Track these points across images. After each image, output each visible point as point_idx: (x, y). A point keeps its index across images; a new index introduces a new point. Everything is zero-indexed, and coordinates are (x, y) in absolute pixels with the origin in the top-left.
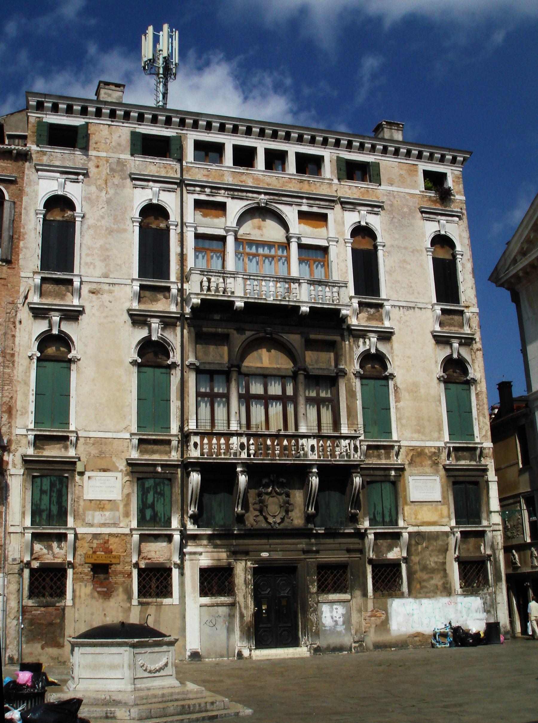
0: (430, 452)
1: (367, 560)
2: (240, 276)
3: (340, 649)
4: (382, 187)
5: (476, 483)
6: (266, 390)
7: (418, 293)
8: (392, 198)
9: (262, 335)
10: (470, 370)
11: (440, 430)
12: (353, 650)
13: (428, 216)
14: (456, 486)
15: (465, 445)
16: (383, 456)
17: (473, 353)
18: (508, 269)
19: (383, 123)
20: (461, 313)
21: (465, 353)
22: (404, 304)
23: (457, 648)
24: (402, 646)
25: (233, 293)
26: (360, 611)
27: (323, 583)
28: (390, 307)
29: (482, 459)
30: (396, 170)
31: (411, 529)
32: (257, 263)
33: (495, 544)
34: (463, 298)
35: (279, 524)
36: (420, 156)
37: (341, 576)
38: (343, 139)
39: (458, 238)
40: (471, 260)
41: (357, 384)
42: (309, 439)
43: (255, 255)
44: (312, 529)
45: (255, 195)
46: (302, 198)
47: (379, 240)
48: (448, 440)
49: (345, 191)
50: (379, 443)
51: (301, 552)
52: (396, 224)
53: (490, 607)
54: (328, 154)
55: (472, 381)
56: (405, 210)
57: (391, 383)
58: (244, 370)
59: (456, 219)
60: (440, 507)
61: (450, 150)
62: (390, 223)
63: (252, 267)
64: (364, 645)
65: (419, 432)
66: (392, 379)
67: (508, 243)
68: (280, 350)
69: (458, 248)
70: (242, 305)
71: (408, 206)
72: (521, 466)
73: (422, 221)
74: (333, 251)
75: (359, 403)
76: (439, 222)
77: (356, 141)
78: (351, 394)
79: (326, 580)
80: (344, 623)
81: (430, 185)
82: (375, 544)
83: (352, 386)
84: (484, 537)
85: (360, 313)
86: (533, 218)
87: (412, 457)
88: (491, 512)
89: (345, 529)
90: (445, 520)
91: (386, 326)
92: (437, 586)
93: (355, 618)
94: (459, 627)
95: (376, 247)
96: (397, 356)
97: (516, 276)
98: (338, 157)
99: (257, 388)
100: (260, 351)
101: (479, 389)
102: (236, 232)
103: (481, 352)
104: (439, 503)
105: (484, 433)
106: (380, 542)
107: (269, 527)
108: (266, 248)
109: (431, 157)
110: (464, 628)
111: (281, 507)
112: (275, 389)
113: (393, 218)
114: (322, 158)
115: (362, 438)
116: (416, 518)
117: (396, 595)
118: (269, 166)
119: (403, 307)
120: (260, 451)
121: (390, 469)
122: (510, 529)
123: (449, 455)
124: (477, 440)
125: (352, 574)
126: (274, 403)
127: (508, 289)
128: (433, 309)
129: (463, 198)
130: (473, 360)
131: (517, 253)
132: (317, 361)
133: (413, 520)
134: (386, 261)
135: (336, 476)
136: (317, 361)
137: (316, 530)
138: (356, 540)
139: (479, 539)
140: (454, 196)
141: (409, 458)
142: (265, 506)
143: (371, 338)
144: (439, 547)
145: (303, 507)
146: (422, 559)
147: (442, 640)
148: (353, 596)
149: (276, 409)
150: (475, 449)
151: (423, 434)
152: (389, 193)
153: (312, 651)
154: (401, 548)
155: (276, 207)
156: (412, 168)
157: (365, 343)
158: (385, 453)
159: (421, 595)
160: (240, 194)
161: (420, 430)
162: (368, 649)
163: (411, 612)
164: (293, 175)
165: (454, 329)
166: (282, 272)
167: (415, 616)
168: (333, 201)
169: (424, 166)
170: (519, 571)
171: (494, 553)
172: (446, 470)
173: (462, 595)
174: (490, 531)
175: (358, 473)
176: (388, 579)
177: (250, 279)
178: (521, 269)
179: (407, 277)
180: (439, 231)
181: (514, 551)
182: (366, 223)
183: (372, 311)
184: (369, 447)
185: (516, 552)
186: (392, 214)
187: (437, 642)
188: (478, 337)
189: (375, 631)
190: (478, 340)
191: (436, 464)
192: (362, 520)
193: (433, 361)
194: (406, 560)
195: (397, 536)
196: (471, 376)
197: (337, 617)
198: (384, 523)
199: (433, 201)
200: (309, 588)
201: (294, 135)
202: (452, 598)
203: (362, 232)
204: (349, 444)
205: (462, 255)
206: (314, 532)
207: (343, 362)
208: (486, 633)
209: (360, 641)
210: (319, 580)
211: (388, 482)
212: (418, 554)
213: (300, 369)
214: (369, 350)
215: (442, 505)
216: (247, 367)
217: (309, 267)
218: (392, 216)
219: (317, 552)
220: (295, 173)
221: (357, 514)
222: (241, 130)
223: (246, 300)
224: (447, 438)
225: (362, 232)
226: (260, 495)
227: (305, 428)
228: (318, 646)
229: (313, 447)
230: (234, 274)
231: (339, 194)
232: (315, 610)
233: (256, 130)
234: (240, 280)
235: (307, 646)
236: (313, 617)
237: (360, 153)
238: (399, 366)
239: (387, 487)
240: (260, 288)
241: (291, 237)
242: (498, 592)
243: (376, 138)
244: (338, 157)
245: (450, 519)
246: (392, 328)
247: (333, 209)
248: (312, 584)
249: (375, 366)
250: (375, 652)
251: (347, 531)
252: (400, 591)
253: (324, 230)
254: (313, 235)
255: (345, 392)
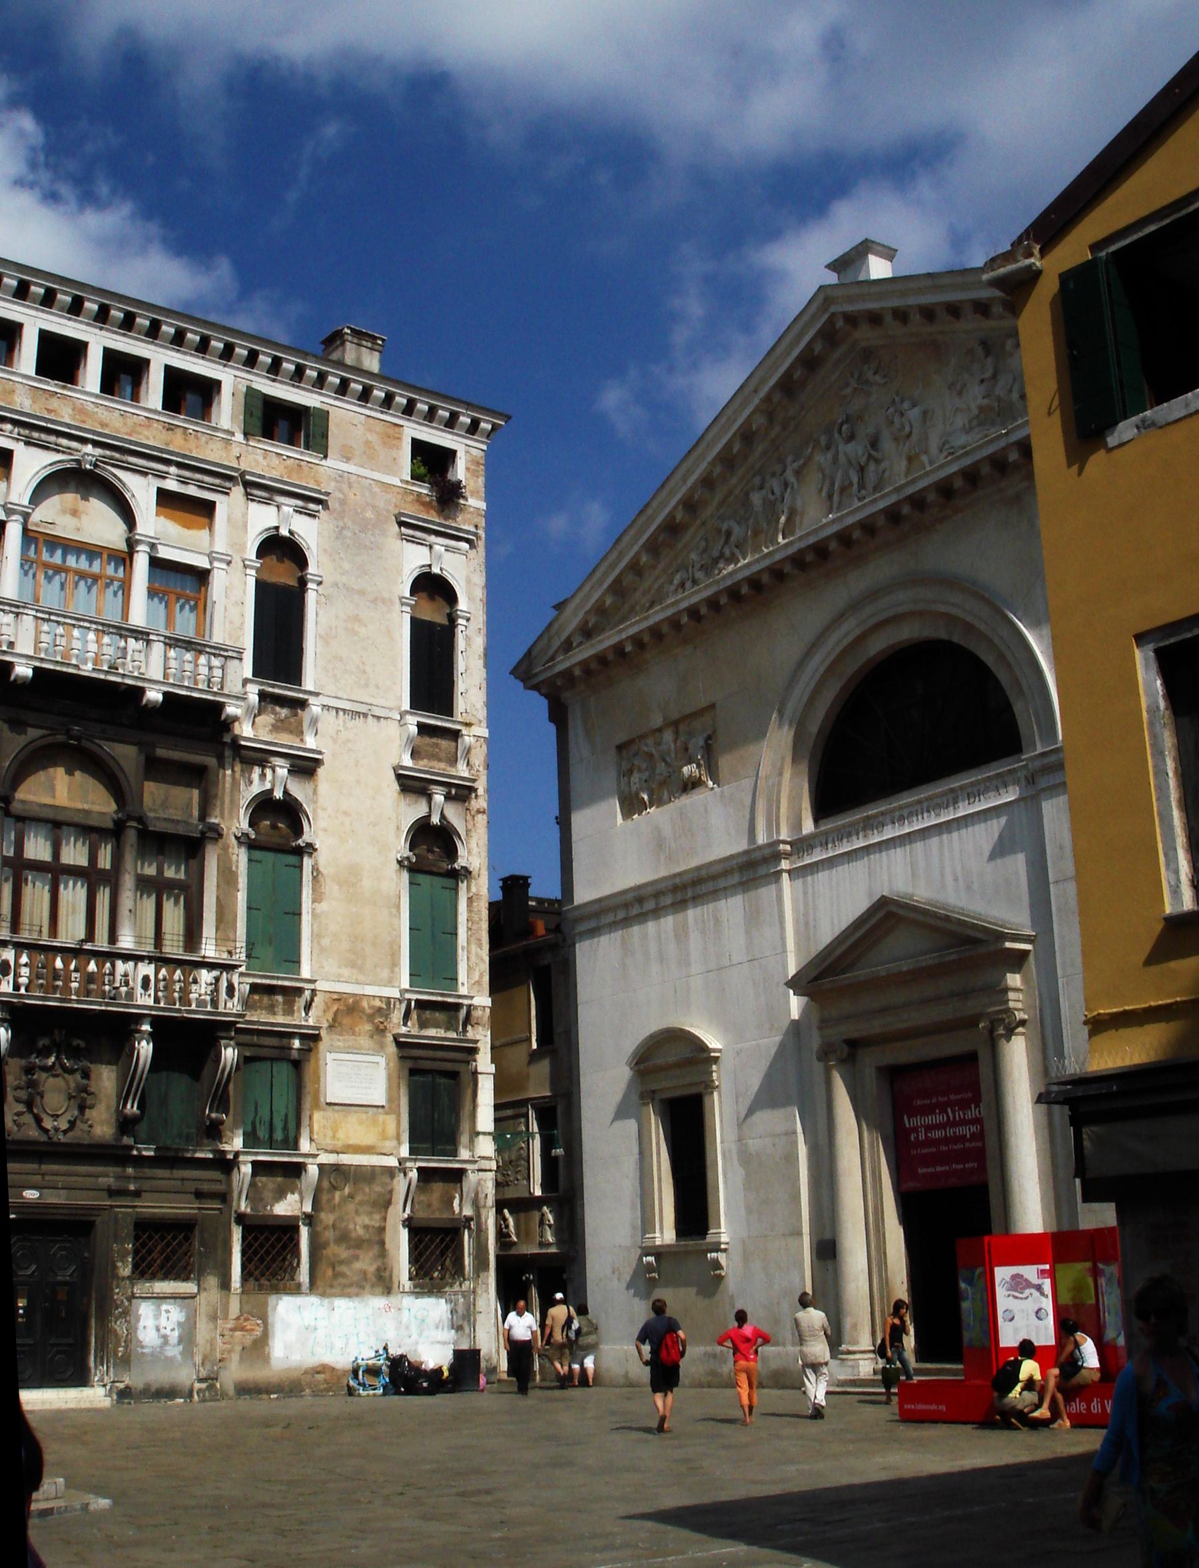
0: (371, 1007)
1: (234, 1215)
2: (30, 612)
3: (170, 1393)
4: (329, 462)
5: (454, 1075)
6: (56, 854)
7: (377, 687)
8: (345, 487)
9: (61, 738)
10: (461, 851)
11: (395, 964)
12: (196, 1396)
13: (410, 532)
14: (416, 1078)
15: (440, 999)
16: (279, 1009)
17: (469, 817)
18: (552, 659)
19: (347, 331)
20: (455, 735)
21: (454, 815)
22: (347, 706)
23: (396, 1397)
24: (291, 1391)
25: (11, 644)
26: (213, 1318)
27: (143, 1259)
28: (319, 709)
29: (469, 1028)
30: (360, 432)
31: (325, 1158)
32: (62, 586)
33: (482, 1196)
34: (460, 705)
35: (65, 1132)
36: (409, 410)
37: (180, 1244)
38: (264, 353)
39: (463, 583)
40: (484, 631)
41: (241, 858)
42: (140, 964)
43: (58, 570)
44: (131, 1148)
45: (74, 444)
46: (168, 462)
47: (312, 569)
48: (407, 986)
49: (256, 461)
50: (274, 982)
51: (105, 1194)
52: (348, 541)
53: (463, 1320)
54: (231, 381)
55: (463, 872)
56: (369, 514)
57: (307, 862)
58: (16, 807)
59: (465, 546)
60: (381, 1118)
61: (469, 405)
62: (337, 538)
63: (51, 595)
64: (218, 1385)
65: (353, 965)
66: (310, 855)
67: (560, 607)
68: (93, 775)
69: (463, 605)
70: (29, 673)
71: (374, 507)
72: (535, 1046)
73: (399, 542)
74: (219, 581)
75: (242, 897)
76: (431, 547)
77: (288, 361)
78: (227, 877)
79: (150, 1252)
80: (180, 1341)
81: (422, 470)
82: (252, 1185)
83: (230, 860)
84: (461, 1181)
85: (259, 713)
86: (616, 565)
87: (336, 1014)
88: (478, 1134)
89: (195, 1151)
90: (389, 1145)
91: (308, 746)
92: (365, 1273)
93: (203, 1331)
94: (403, 1357)
95: (303, 583)
96: (324, 809)
97: (567, 674)
98: (250, 389)
99: (37, 848)
100: (51, 770)
101: (474, 889)
102: (26, 516)
103: (485, 817)
104: (380, 1110)
105: (476, 978)
106: (262, 1180)
107: (44, 1138)
108: (83, 557)
109: (430, 416)
110: (412, 1358)
111: (70, 1097)
112: (75, 854)
113: (343, 528)
114: (217, 384)
115: (242, 969)
116: (334, 1137)
117: (284, 1289)
118: (109, 386)
119: (344, 710)
120: (41, 981)
121: (291, 1035)
122: (510, 1166)
123: (407, 1016)
124: (463, 991)
125: (203, 1244)
126: (71, 883)
127: (546, 696)
128: (401, 723)
129: (483, 505)
130: (468, 831)
131: (575, 629)
132: (167, 803)
133: (328, 1141)
134: (321, 613)
135: (187, 1041)
136: (165, 805)
137: (138, 1149)
138: (216, 1175)
139: (452, 1185)
140: (465, 498)
141: (330, 1016)
142: (38, 1094)
143: (278, 769)
144: (373, 1196)
145: (114, 1102)
146: (341, 1218)
147: (369, 1380)
148: (202, 1286)
149: (74, 895)
150: (457, 1007)
151: (361, 969)
152: (342, 476)
153: (115, 1397)
154: (301, 1194)
155: (115, 476)
156: (391, 431)
157: (263, 776)
158: (284, 1003)
159: (333, 1291)
160: (43, 436)
161: (355, 961)
162: (224, 1395)
163: (313, 1323)
164: (155, 412)
165: (439, 766)
166: (112, 615)
167: (322, 1330)
168: (229, 478)
169: (414, 430)
170: (513, 1251)
171: (478, 1215)
172: (399, 1045)
173: (413, 1293)
174: (473, 1172)
175: (231, 1039)
176: (272, 1255)
177: (49, 620)
178: (579, 663)
179: (357, 651)
180: (430, 566)
181: (506, 1211)
182: (291, 532)
183: (284, 712)
184: (255, 988)
185: (511, 1213)
186: (343, 518)
187: (359, 1384)
188: (481, 786)
189: (241, 1360)
190: (481, 791)
191: (380, 1031)
192: (229, 1133)
193: (392, 828)
194: (310, 1219)
195: (296, 1170)
196: (461, 862)
197: (169, 1329)
198: (271, 1143)
199: (423, 504)
200: (115, 1267)
201: (168, 330)
202: (394, 1300)
203: (280, 548)
204: (217, 979)
205: (468, 620)
206: (135, 1153)
207: (217, 812)
208: (452, 1368)
209: (210, 1379)
210: (136, 1252)
211: (286, 1059)
212: (333, 1210)
213: (130, 818)
214: (271, 791)
215: (387, 1113)
216: (23, 802)
217: (166, 606)
218: (341, 524)
219: (137, 1194)
220: (160, 408)
221: (222, 1122)
222: (61, 301)
223: (38, 664)
224: (405, 984)
225: (280, 548)
226: (29, 1070)
227: (131, 939)
228: (127, 1387)
229: (146, 980)
230: (18, 607)
231: (243, 466)
232: (126, 1313)
233: (91, 306)
234: (28, 621)
235: (104, 1386)
236: (120, 1327)
237: (293, 386)
238: (325, 830)
239: (283, 1072)
240: (69, 642)
241: (138, 542)
242: (479, 1291)
243: (325, 360)
244: (250, 389)
245: (400, 1143)
246: (320, 753)
247: (227, 494)
248: (123, 1259)
249: (280, 824)
250: (240, 1402)
251: (199, 1155)
252: (293, 1279)
253: (205, 533)
254: (181, 543)
255: (215, 872)
